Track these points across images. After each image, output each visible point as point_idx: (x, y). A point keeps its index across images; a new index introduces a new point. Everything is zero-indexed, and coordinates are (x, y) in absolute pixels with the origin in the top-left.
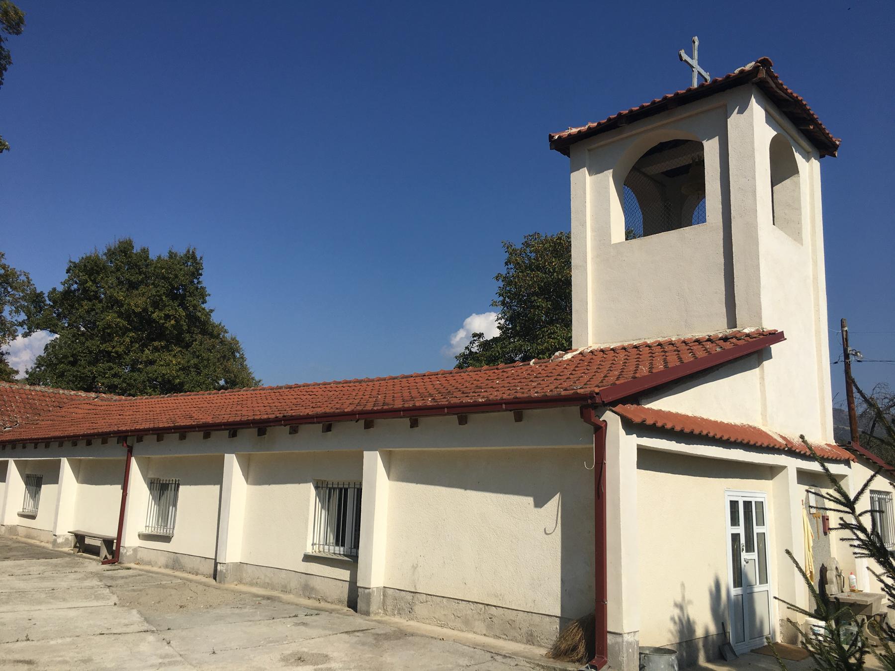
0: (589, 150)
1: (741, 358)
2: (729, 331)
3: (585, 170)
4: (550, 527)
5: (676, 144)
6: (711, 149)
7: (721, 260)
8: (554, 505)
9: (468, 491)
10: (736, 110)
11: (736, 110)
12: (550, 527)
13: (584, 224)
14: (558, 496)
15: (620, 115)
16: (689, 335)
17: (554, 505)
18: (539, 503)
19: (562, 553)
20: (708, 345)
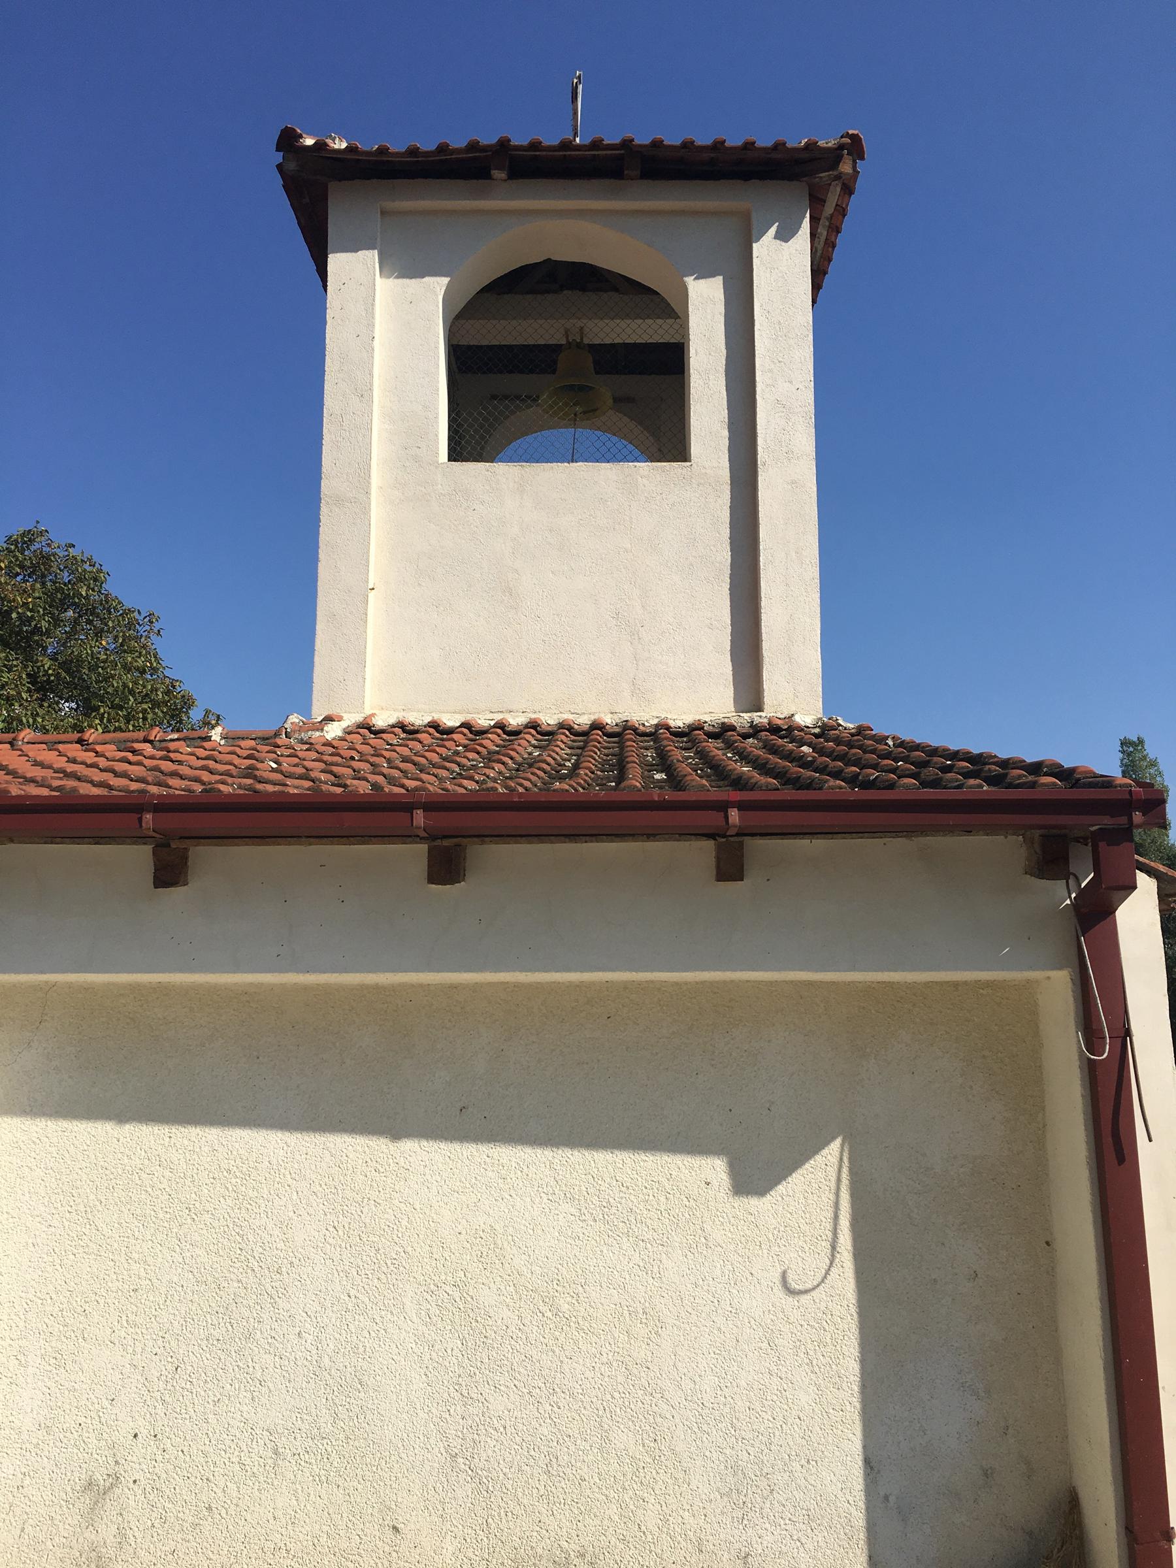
0: (383, 213)
1: (218, 838)
2: (744, 719)
3: (371, 257)
4: (807, 1265)
5: (584, 279)
6: (705, 300)
7: (724, 556)
8: (817, 1186)
9: (408, 1145)
10: (773, 231)
11: (773, 231)
12: (807, 1265)
13: (365, 394)
14: (836, 1145)
15: (504, 144)
16: (646, 716)
17: (817, 1186)
18: (753, 1177)
19: (863, 1362)
20: (714, 748)
